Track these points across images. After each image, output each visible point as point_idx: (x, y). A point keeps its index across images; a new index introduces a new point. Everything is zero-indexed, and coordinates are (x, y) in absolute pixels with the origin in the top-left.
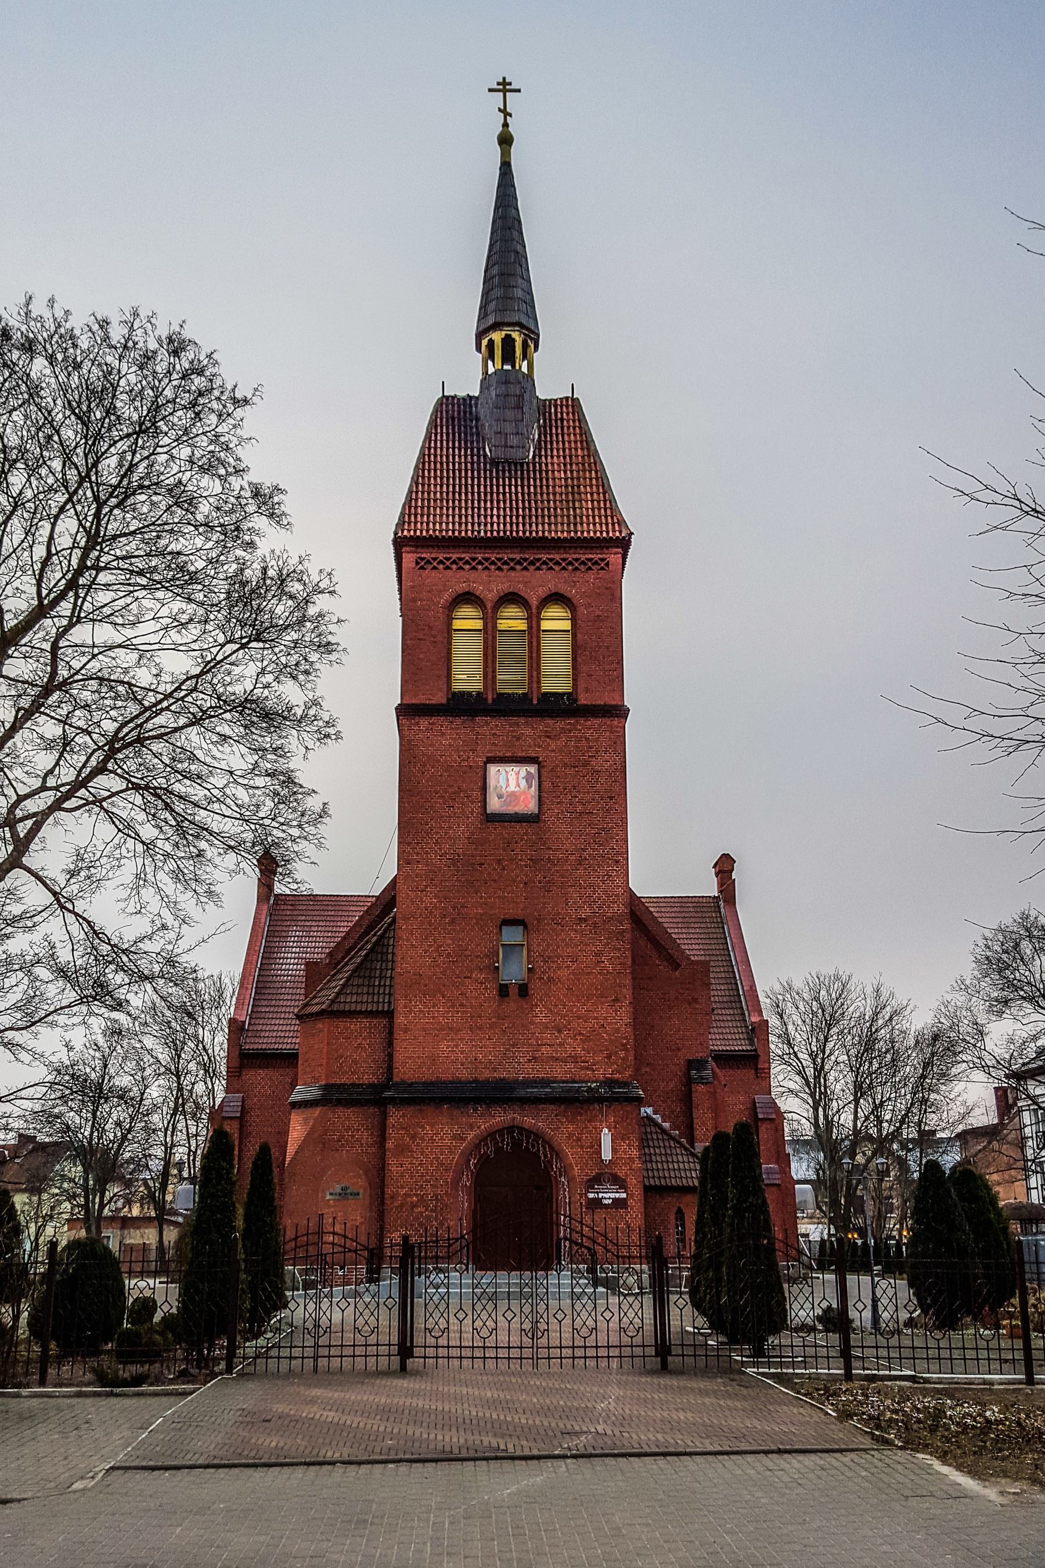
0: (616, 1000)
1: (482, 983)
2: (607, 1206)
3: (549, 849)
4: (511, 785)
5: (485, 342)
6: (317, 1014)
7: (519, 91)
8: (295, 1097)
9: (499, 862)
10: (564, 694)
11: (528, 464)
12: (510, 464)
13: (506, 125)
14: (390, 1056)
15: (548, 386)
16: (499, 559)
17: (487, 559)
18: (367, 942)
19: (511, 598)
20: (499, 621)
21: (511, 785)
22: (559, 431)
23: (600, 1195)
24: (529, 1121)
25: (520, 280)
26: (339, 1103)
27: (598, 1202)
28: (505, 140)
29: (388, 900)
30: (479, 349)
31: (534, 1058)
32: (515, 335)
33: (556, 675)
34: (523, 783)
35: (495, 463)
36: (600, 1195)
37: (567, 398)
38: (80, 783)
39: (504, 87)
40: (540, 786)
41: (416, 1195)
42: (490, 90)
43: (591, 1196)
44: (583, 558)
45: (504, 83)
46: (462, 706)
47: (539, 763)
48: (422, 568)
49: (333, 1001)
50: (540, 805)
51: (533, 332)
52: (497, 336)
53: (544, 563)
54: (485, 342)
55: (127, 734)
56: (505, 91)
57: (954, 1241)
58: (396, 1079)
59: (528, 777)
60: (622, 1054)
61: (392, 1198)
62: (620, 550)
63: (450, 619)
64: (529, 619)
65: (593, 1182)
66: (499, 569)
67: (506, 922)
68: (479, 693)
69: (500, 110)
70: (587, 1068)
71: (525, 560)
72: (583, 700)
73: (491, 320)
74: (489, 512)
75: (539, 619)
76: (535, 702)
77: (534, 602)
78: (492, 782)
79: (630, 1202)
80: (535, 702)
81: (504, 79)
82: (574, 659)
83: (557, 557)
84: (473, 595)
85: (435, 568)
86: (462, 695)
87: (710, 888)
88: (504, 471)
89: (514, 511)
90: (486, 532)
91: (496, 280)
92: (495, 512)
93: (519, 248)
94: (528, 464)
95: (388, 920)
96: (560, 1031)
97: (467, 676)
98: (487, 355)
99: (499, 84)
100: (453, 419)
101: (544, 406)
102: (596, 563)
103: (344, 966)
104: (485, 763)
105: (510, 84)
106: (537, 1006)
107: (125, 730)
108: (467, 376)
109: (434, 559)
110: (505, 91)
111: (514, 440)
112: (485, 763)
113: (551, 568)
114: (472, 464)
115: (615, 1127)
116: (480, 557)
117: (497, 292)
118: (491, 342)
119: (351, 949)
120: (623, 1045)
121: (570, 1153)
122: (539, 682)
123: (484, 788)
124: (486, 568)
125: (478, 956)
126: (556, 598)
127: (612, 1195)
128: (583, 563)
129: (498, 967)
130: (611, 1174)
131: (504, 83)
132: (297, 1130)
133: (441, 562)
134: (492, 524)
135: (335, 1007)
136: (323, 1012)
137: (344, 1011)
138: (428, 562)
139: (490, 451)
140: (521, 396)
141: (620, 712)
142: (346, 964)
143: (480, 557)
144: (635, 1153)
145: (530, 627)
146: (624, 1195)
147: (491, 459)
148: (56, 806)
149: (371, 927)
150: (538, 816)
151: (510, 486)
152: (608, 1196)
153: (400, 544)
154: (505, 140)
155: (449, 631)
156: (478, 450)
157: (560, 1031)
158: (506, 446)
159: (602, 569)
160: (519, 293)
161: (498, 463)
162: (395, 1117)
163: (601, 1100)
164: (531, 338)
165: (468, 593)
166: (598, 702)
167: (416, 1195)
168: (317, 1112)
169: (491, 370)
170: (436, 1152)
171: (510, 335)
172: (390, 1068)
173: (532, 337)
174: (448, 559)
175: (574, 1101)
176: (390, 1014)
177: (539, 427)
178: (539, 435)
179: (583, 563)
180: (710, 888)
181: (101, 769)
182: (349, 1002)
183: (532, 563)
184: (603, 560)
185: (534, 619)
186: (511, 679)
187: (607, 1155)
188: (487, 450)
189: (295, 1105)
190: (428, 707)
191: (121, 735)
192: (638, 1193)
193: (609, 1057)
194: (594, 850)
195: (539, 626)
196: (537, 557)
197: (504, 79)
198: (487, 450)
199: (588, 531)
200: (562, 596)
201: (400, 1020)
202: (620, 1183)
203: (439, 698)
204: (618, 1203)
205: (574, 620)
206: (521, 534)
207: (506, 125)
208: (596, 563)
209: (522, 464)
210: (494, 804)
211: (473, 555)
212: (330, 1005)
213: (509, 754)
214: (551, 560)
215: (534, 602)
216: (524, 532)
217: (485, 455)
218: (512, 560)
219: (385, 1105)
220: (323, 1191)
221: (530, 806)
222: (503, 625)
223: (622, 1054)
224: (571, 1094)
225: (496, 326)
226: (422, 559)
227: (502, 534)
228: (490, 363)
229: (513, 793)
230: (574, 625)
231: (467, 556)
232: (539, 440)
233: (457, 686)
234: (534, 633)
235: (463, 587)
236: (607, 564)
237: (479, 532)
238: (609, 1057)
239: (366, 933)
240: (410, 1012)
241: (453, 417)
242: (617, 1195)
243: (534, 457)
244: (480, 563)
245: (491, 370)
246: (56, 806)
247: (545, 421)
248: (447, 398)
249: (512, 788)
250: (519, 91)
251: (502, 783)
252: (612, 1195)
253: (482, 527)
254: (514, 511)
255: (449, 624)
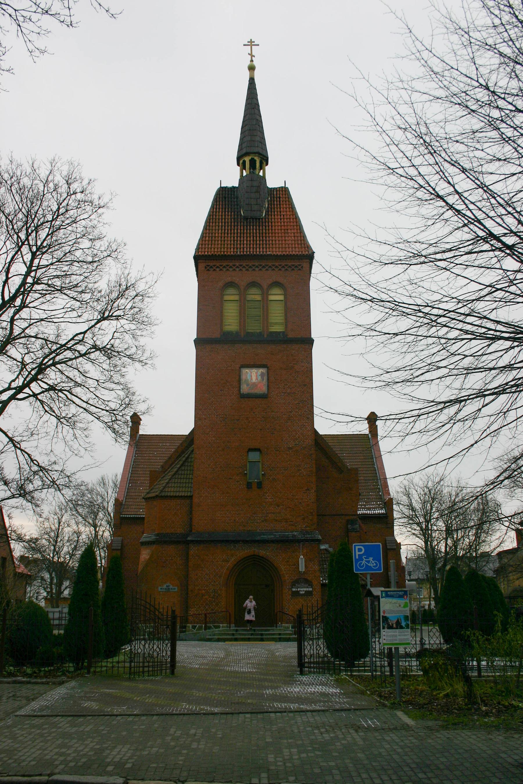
0: (308, 490)
1: (238, 481)
2: (302, 595)
3: (272, 412)
4: (253, 377)
5: (241, 162)
6: (153, 497)
7: (258, 45)
8: (143, 540)
9: (247, 419)
10: (281, 332)
11: (262, 219)
12: (253, 219)
13: (252, 61)
14: (191, 519)
15: (273, 178)
16: (247, 265)
17: (241, 265)
18: (180, 460)
19: (253, 284)
20: (247, 296)
21: (253, 377)
22: (278, 203)
23: (299, 589)
24: (262, 552)
25: (259, 133)
26: (165, 542)
27: (298, 592)
28: (252, 68)
29: (188, 442)
30: (238, 165)
31: (265, 520)
32: (256, 158)
33: (277, 322)
34: (259, 378)
35: (246, 218)
36: (299, 589)
37: (282, 187)
38: (26, 385)
39: (251, 44)
40: (268, 379)
41: (205, 590)
42: (244, 45)
43: (294, 590)
44: (290, 264)
45: (251, 42)
46: (228, 339)
47: (268, 368)
48: (208, 270)
49: (162, 491)
50: (268, 389)
51: (265, 156)
52: (247, 159)
53: (270, 267)
54: (241, 162)
55: (47, 362)
56: (251, 46)
57: (471, 595)
58: (193, 531)
59: (262, 375)
60: (311, 518)
61: (192, 591)
62: (308, 260)
63: (222, 295)
64: (262, 294)
65: (295, 583)
66: (247, 270)
67: (250, 450)
68: (237, 333)
69: (249, 54)
70: (293, 525)
71: (261, 265)
72: (291, 335)
73: (244, 151)
74: (242, 242)
75: (268, 295)
76: (265, 336)
77: (265, 287)
78: (243, 377)
79: (314, 593)
80: (265, 336)
81: (251, 40)
82: (286, 315)
83: (277, 264)
84: (234, 283)
85: (214, 270)
86: (229, 333)
87: (363, 428)
88: (250, 223)
89: (252, 242)
90: (240, 252)
91: (247, 133)
92: (245, 242)
93: (258, 117)
94: (262, 219)
95: (191, 449)
96: (278, 506)
97: (231, 322)
98: (242, 167)
99: (248, 42)
100: (225, 198)
101: (271, 191)
102: (296, 267)
103: (168, 473)
104: (240, 368)
105: (254, 42)
106: (266, 493)
107: (46, 360)
108: (232, 177)
109: (215, 266)
110: (251, 46)
111: (255, 208)
112: (240, 368)
113: (274, 270)
114: (234, 219)
115: (307, 555)
116: (237, 264)
117: (248, 138)
118: (244, 162)
119: (172, 464)
120: (311, 513)
121: (283, 568)
122: (267, 326)
123: (239, 381)
124: (241, 270)
125: (236, 468)
126: (277, 284)
127: (305, 589)
128: (290, 267)
129: (246, 474)
130: (304, 578)
131: (251, 42)
132: (145, 554)
133: (218, 267)
134: (243, 248)
135: (163, 494)
136: (157, 496)
137: (167, 496)
138: (211, 267)
139: (244, 213)
140: (259, 187)
141: (310, 342)
142: (169, 472)
143: (237, 264)
144: (317, 568)
145: (263, 299)
146: (311, 589)
147: (244, 217)
148: (13, 397)
149: (183, 452)
150: (267, 395)
151: (253, 230)
152: (303, 590)
153: (197, 258)
154: (252, 68)
155: (222, 301)
156: (238, 212)
157: (278, 506)
158: (251, 211)
159: (299, 270)
160: (258, 139)
161: (247, 219)
162: (193, 550)
163: (299, 541)
164: (264, 159)
165: (231, 282)
166: (298, 337)
167: (205, 590)
168: (154, 547)
169: (245, 174)
170: (215, 568)
171: (253, 158)
172: (191, 525)
173: (265, 160)
174: (221, 265)
175: (286, 542)
176: (191, 497)
177: (268, 201)
178: (268, 205)
179: (290, 267)
180: (363, 428)
181: (35, 379)
182: (171, 491)
183: (264, 267)
184: (300, 265)
185: (265, 295)
186: (254, 327)
187: (302, 568)
188: (242, 212)
189: (143, 544)
190: (210, 341)
191: (44, 362)
192: (318, 588)
193: (304, 519)
194: (296, 412)
195: (267, 298)
196: (267, 264)
197: (251, 40)
198: (242, 212)
199: (290, 251)
200: (280, 283)
201: (195, 500)
202: (308, 583)
203: (217, 335)
204: (308, 594)
205: (285, 295)
206: (258, 253)
207: (252, 61)
208: (296, 267)
209: (259, 219)
210: (245, 389)
211: (234, 264)
212: (160, 493)
213: (252, 363)
214: (273, 265)
215: (265, 287)
216: (260, 252)
217: (241, 215)
218: (254, 265)
219: (188, 544)
220: (157, 588)
221: (263, 389)
222: (249, 297)
223: (311, 518)
224: (285, 538)
225: (247, 154)
226: (208, 266)
227: (248, 253)
228: (244, 171)
229: (254, 383)
230: (285, 298)
231: (231, 264)
232: (268, 208)
233: (227, 328)
234: (265, 302)
235: (229, 279)
236: (302, 267)
237: (237, 252)
238: (304, 519)
239: (180, 456)
240: (201, 496)
241: (224, 196)
242: (307, 589)
243: (265, 215)
244: (238, 267)
245: (245, 174)
246: (13, 397)
247: (271, 198)
248: (223, 187)
249: (254, 380)
250: (258, 45)
251: (249, 378)
252: (305, 589)
253: (239, 250)
254: (252, 242)
255: (222, 297)
